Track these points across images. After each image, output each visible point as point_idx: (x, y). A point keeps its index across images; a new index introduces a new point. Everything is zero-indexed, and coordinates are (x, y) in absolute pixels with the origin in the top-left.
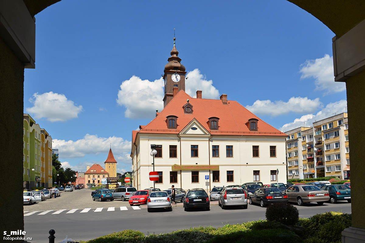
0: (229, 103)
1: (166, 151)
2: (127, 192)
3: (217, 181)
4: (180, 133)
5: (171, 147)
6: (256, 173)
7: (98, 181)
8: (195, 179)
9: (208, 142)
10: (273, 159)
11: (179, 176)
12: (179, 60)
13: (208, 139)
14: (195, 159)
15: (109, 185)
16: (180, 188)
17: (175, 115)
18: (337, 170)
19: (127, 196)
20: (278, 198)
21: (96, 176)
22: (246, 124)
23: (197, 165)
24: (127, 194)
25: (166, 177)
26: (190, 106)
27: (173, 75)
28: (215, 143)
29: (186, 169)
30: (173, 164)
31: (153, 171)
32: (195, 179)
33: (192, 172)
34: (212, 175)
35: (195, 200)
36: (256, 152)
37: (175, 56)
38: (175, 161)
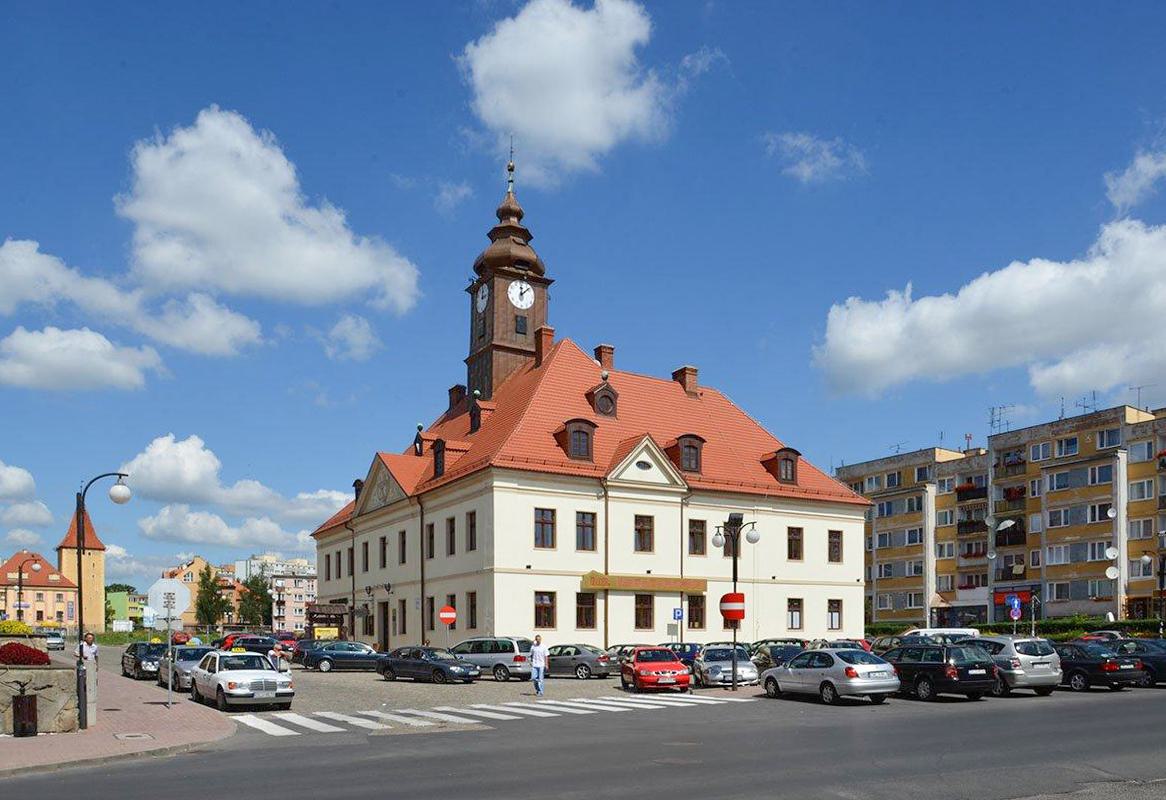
0: (701, 394)
1: (566, 529)
2: (517, 652)
3: (697, 624)
4: (607, 474)
5: (581, 515)
6: (795, 605)
7: (38, 612)
8: (644, 618)
9: (680, 509)
10: (834, 566)
11: (600, 603)
12: (526, 236)
13: (679, 500)
14: (644, 556)
15: (316, 629)
16: (732, 641)
17: (697, 434)
18: (910, 605)
19: (518, 665)
20: (976, 675)
21: (29, 595)
22: (554, 435)
23: (649, 575)
24: (517, 659)
25: (566, 610)
26: (610, 394)
27: (513, 283)
28: (695, 512)
29: (622, 586)
30: (587, 570)
31: (732, 592)
32: (644, 618)
33: (636, 596)
34: (686, 604)
35: (971, 672)
36: (795, 545)
37: (514, 220)
38: (591, 562)
